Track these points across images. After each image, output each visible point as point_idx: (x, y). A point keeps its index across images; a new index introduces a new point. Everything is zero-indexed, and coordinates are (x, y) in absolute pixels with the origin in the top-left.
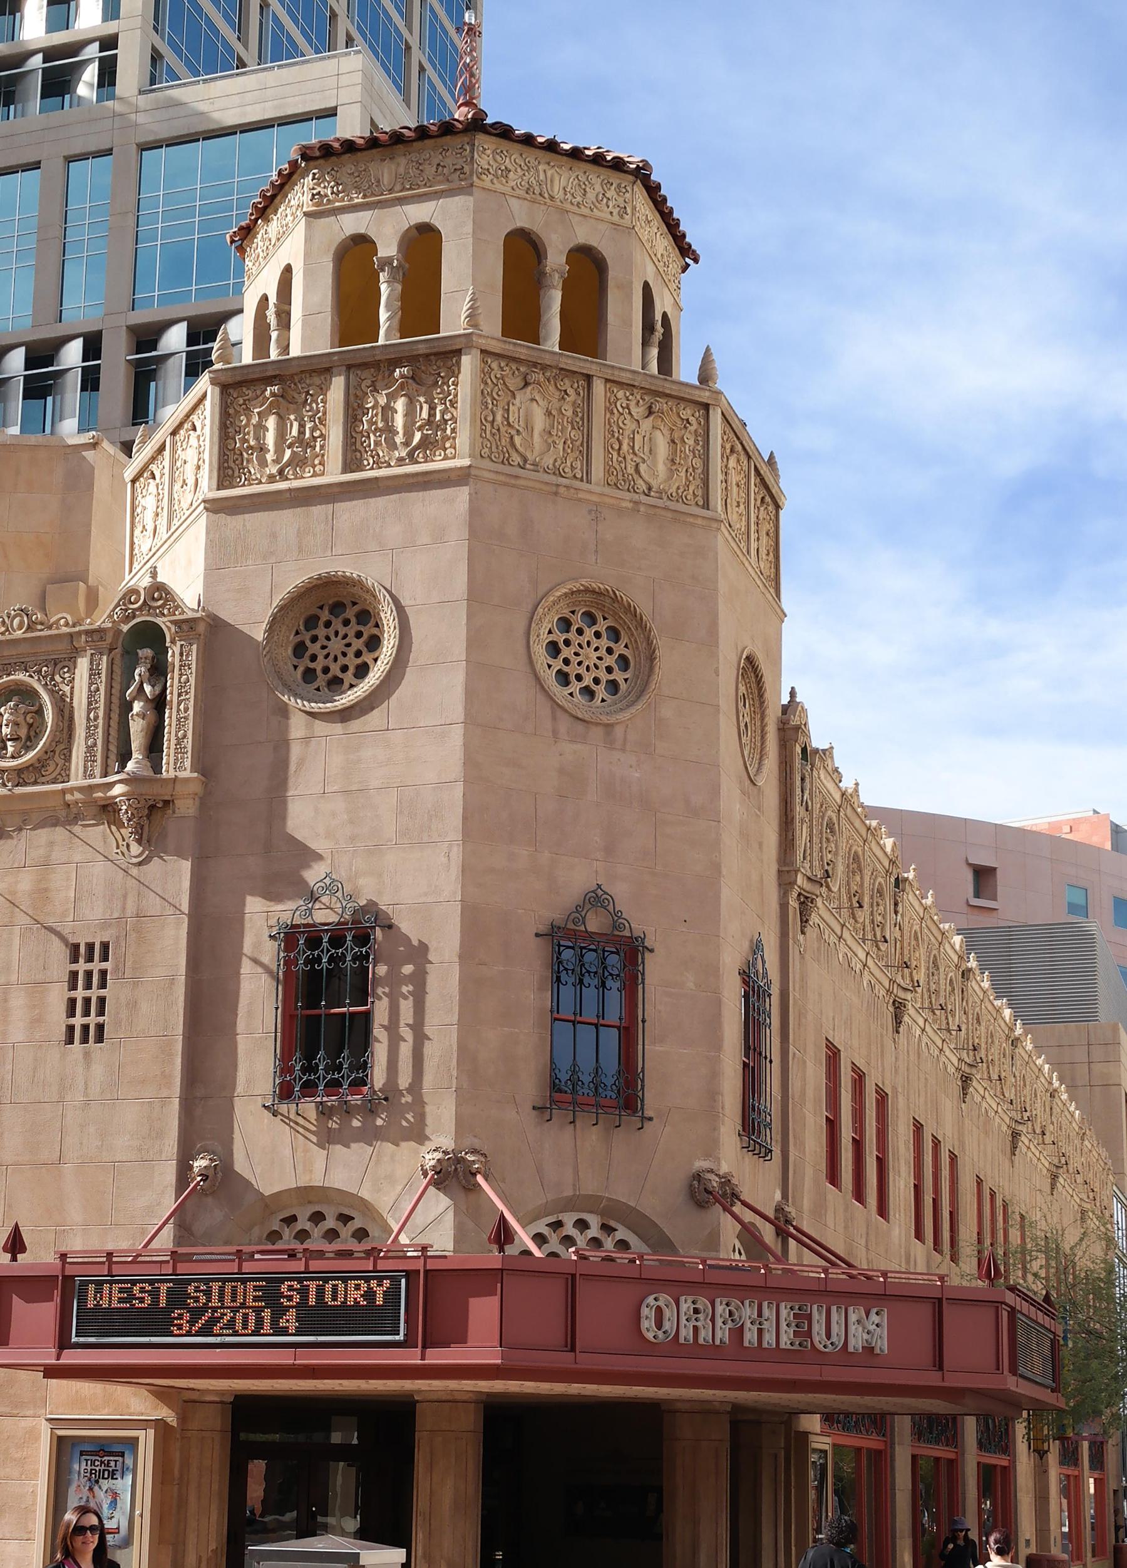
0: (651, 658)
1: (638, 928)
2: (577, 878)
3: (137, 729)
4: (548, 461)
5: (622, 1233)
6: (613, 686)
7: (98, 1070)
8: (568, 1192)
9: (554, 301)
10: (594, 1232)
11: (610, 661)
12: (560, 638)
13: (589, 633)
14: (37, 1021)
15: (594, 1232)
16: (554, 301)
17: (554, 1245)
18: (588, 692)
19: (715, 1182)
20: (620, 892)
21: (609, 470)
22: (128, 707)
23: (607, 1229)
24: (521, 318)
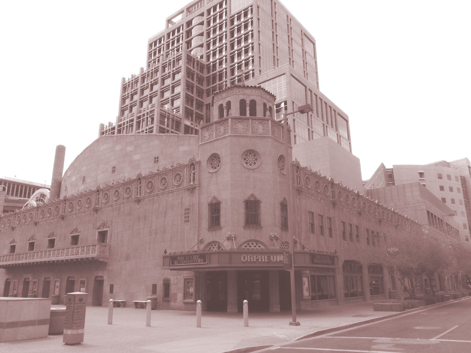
1: (259, 199)
2: (249, 193)
3: (192, 178)
5: (259, 245)
8: (249, 239)
9: (248, 108)
10: (255, 245)
12: (246, 157)
16: (248, 108)
17: (248, 247)
18: (251, 165)
22: (190, 175)
23: (256, 244)
24: (243, 112)
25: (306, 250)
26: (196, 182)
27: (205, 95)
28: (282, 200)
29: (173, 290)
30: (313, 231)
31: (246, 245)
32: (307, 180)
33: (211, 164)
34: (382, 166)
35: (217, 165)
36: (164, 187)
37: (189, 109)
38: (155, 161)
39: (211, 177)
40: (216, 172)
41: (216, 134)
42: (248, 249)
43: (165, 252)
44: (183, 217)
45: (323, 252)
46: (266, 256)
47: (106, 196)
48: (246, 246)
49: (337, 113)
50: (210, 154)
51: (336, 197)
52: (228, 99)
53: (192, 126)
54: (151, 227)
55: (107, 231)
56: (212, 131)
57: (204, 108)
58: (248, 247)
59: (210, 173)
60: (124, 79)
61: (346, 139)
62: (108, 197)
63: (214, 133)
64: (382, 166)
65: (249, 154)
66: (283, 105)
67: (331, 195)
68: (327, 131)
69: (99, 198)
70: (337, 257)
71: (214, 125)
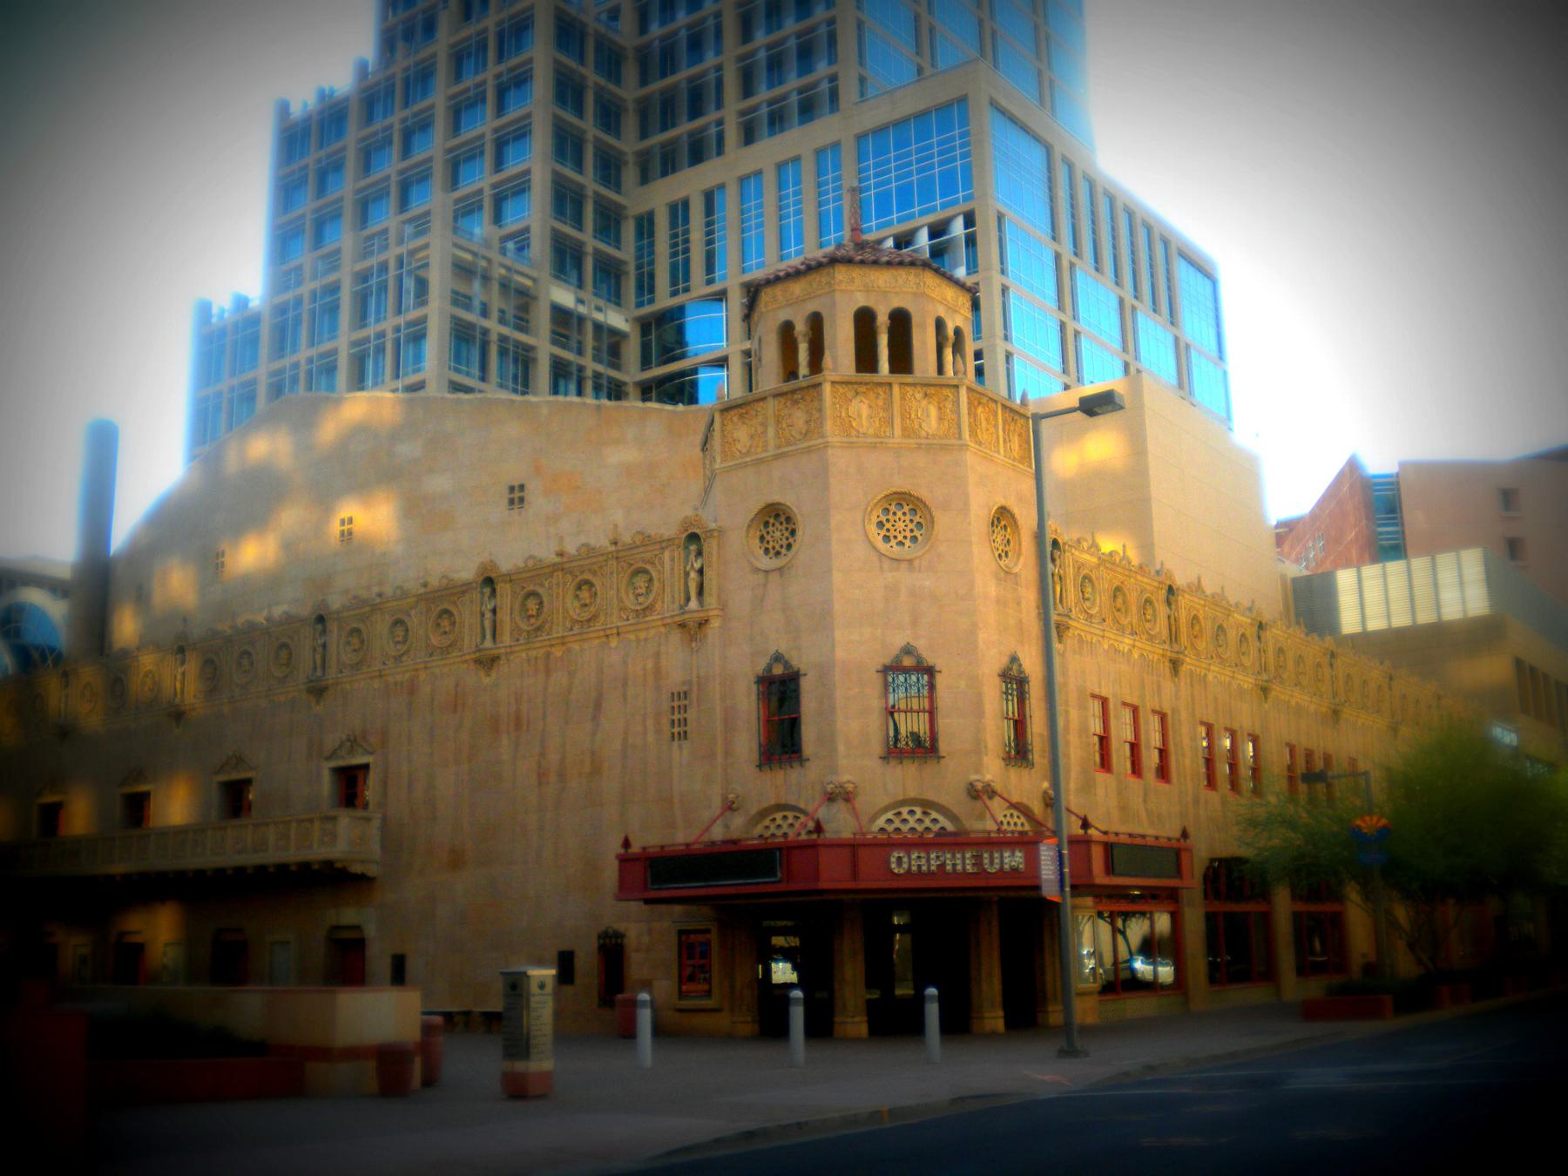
0: (932, 522)
2: (899, 640)
4: (871, 431)
6: (914, 539)
7: (685, 753)
9: (883, 341)
11: (911, 526)
12: (883, 519)
13: (899, 514)
14: (658, 732)
15: (919, 815)
16: (883, 341)
18: (901, 543)
19: (979, 786)
20: (921, 645)
21: (904, 429)
22: (687, 574)
23: (925, 813)
24: (866, 359)
25: (1092, 831)
26: (711, 600)
27: (630, 175)
28: (1005, 660)
29: (636, 966)
30: (1105, 763)
31: (890, 815)
32: (1087, 583)
33: (762, 538)
34: (1353, 466)
35: (785, 542)
36: (586, 616)
37: (566, 236)
38: (512, 502)
39: (765, 586)
40: (780, 569)
41: (777, 436)
42: (898, 830)
43: (626, 844)
44: (665, 722)
45: (1143, 837)
46: (968, 855)
47: (355, 641)
48: (889, 821)
49: (1174, 251)
50: (761, 505)
51: (1184, 638)
52: (812, 307)
53: (582, 309)
54: (543, 755)
55: (366, 767)
56: (764, 425)
57: (629, 231)
58: (897, 824)
59: (757, 570)
60: (284, 109)
61: (1209, 358)
62: (362, 642)
63: (771, 431)
64: (1353, 466)
65: (893, 508)
66: (958, 229)
67: (1165, 632)
68: (1134, 321)
69: (324, 646)
70: (1189, 850)
71: (770, 400)
